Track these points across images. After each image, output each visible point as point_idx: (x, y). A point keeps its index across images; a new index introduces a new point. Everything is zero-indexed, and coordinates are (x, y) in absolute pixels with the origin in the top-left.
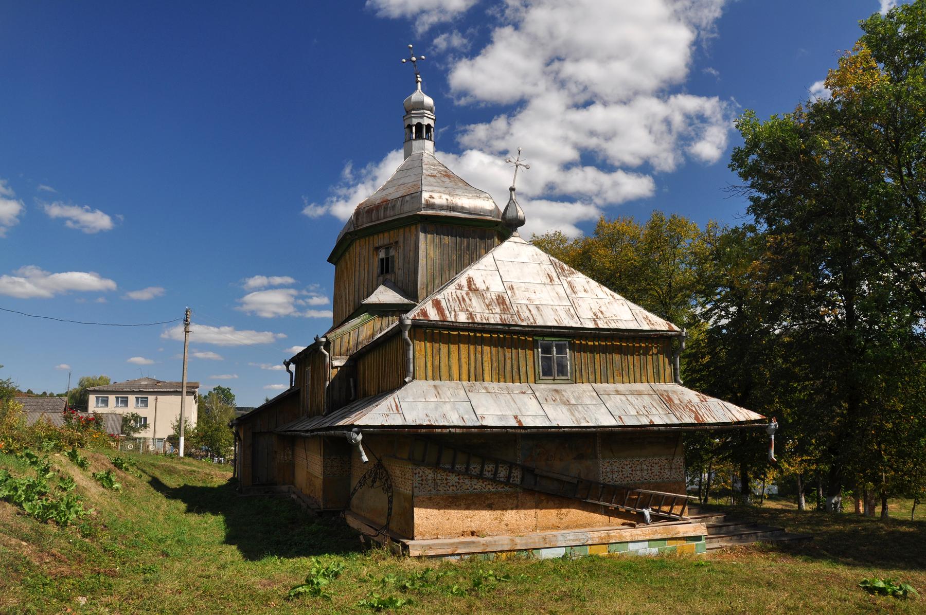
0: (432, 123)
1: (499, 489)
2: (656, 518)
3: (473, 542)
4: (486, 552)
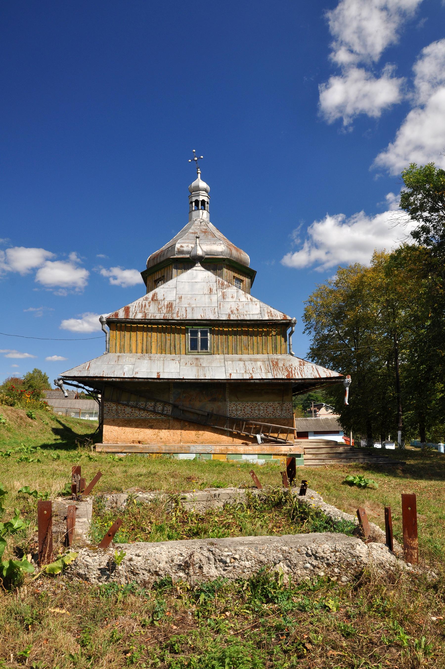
0: (206, 199)
1: (158, 417)
2: (265, 441)
3: (135, 446)
4: (142, 453)
